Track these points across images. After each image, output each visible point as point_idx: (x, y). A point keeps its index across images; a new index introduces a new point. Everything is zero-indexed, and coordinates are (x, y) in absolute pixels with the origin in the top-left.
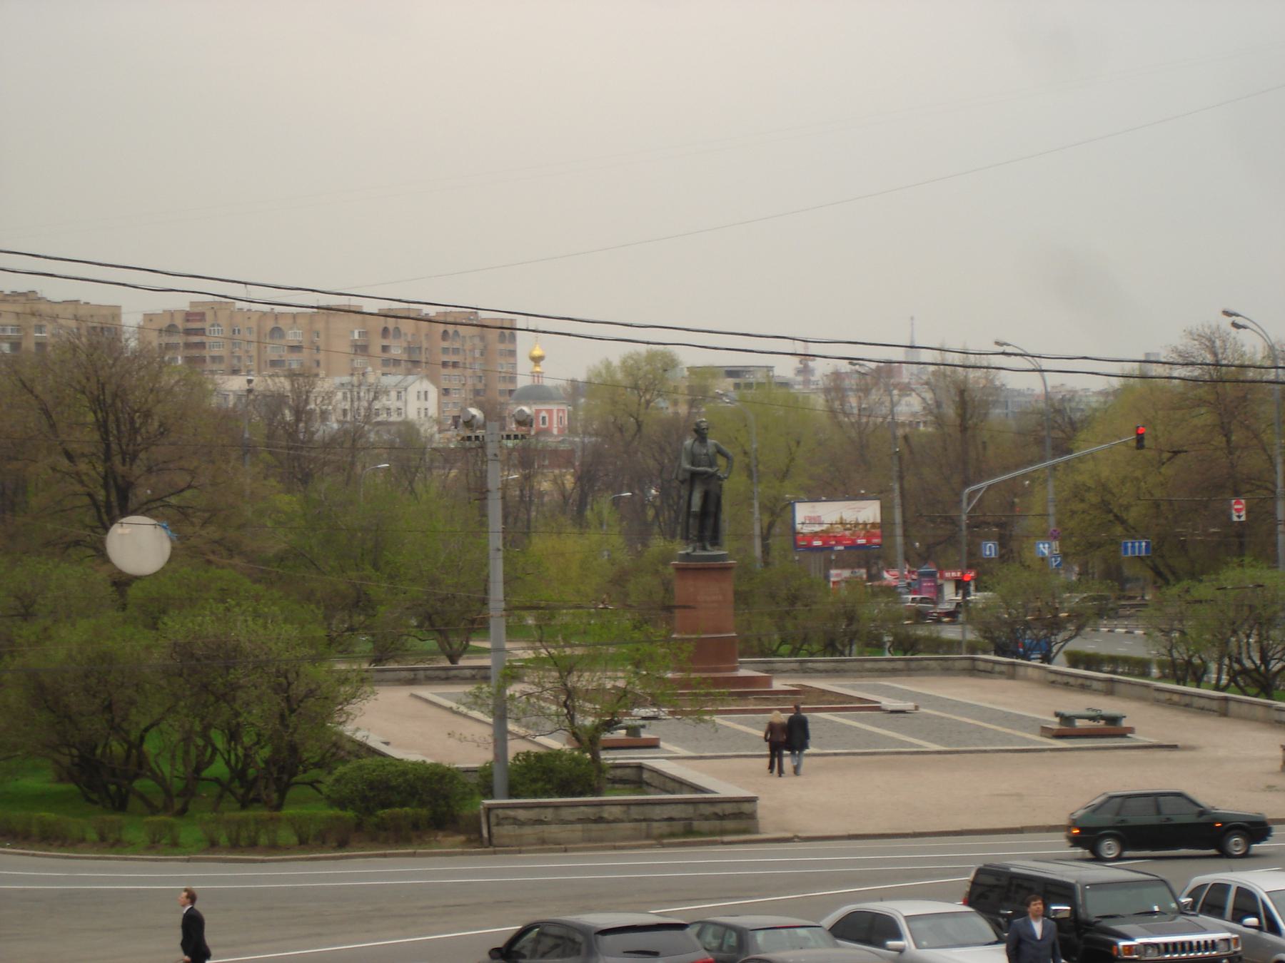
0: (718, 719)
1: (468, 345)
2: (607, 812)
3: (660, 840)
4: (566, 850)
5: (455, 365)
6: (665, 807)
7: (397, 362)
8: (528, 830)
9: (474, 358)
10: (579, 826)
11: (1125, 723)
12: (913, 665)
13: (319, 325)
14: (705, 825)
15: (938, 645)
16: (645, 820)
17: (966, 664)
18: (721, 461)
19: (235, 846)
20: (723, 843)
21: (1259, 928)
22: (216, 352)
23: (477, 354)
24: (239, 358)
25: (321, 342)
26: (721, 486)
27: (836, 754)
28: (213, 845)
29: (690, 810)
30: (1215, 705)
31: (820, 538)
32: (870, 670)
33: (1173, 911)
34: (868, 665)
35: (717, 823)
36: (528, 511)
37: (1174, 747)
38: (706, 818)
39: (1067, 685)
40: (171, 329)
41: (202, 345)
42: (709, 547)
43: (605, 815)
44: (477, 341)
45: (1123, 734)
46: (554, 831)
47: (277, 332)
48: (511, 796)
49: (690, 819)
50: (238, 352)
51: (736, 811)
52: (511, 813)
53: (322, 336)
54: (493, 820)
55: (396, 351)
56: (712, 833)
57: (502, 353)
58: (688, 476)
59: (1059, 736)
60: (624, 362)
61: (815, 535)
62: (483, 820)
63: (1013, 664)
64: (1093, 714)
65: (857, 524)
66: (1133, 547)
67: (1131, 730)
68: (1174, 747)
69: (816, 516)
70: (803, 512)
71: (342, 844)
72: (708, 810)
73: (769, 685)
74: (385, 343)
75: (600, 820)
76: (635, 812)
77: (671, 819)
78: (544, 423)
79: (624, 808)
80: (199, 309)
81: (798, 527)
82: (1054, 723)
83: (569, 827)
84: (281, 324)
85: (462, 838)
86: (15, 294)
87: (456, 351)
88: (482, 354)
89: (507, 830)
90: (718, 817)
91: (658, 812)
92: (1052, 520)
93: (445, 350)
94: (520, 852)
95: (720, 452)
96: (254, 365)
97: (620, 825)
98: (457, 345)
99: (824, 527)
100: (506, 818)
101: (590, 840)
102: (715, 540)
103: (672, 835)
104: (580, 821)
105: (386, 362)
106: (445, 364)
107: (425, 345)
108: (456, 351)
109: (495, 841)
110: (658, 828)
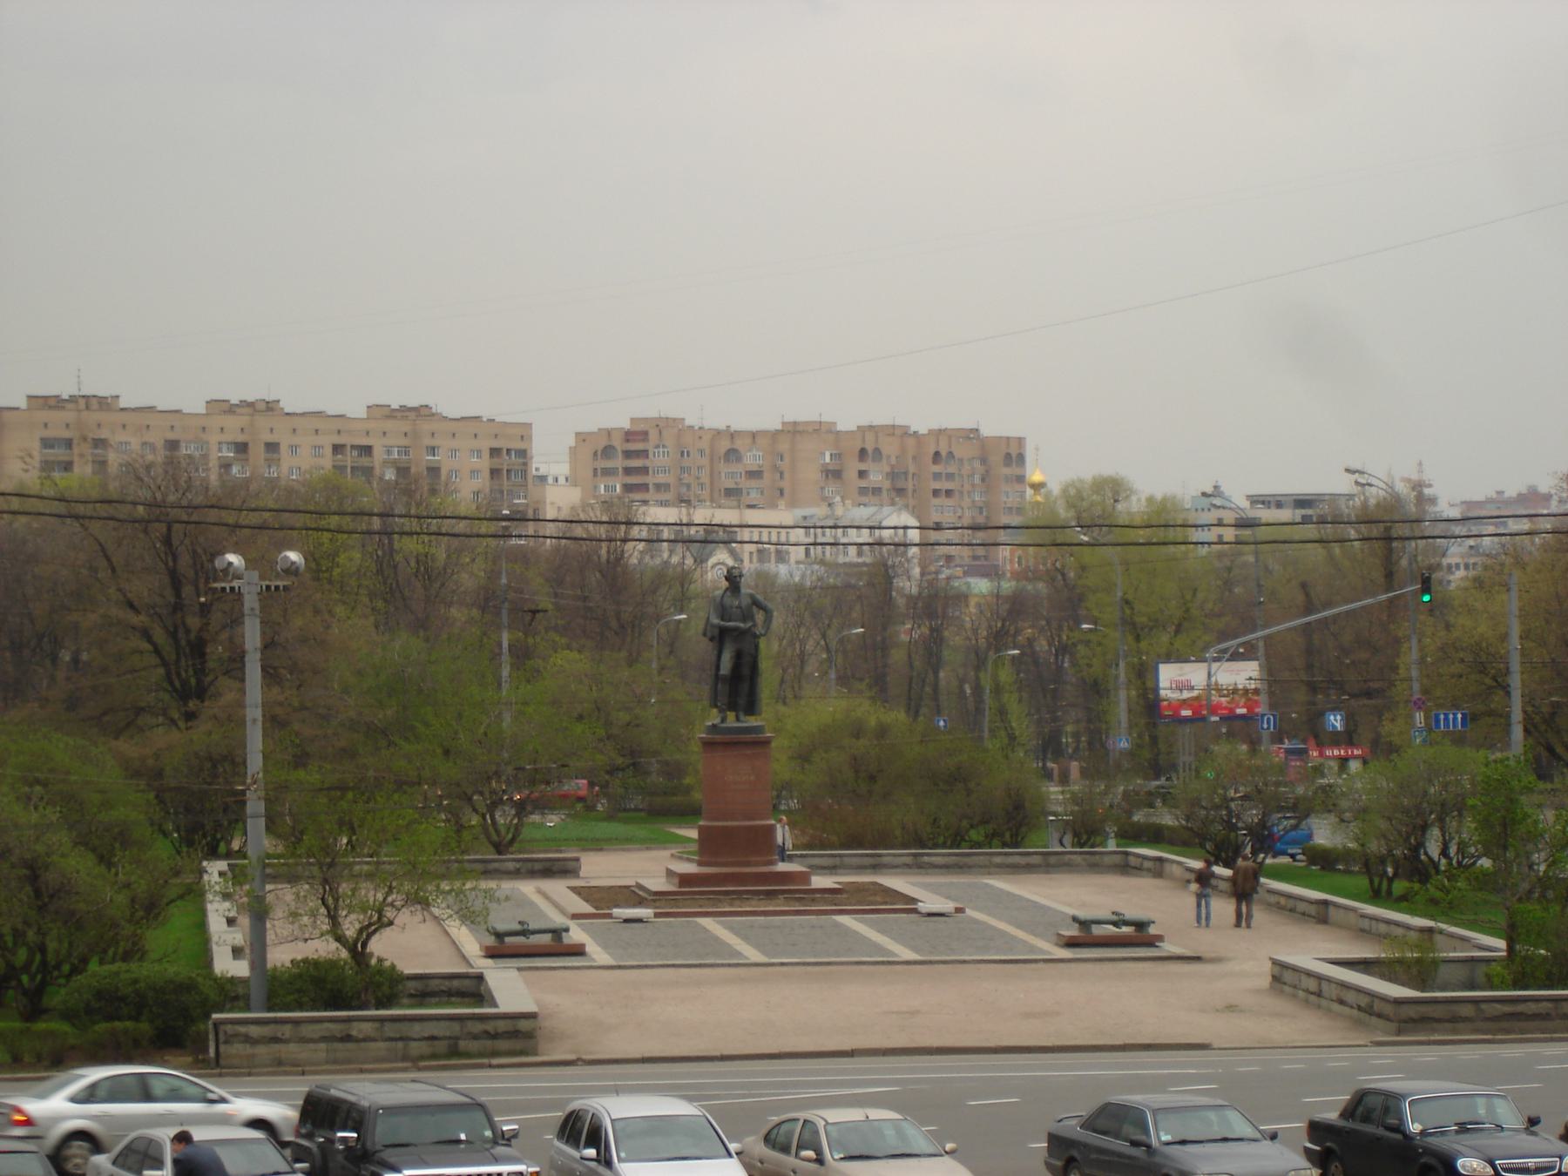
0: (706, 922)
1: (966, 469)
2: (356, 1030)
3: (415, 1062)
4: (303, 1073)
5: (949, 493)
6: (426, 1024)
7: (877, 491)
8: (261, 1050)
9: (973, 485)
10: (323, 1046)
11: (1152, 930)
12: (1053, 860)
13: (784, 446)
14: (474, 1046)
16: (401, 1039)
17: (1117, 859)
18: (760, 617)
20: (490, 1066)
21: (597, 1160)
22: (661, 478)
23: (977, 480)
24: (688, 486)
25: (784, 465)
26: (757, 647)
27: (782, 964)
29: (455, 1028)
30: (1312, 910)
31: (1190, 707)
32: (999, 866)
33: (486, 1140)
34: (998, 860)
35: (489, 1043)
36: (936, 673)
37: (1198, 959)
38: (475, 1037)
40: (608, 451)
41: (644, 471)
42: (742, 717)
43: (354, 1033)
44: (977, 464)
45: (1151, 942)
47: (732, 455)
48: (270, 1010)
49: (457, 1038)
50: (687, 479)
51: (511, 1028)
52: (242, 1029)
53: (787, 460)
54: (222, 1037)
55: (876, 477)
56: (481, 1055)
57: (1008, 479)
58: (716, 632)
59: (1071, 943)
60: (1065, 491)
61: (1184, 703)
62: (211, 1037)
63: (1160, 859)
64: (1115, 918)
65: (1235, 691)
66: (1446, 719)
67: (1160, 938)
68: (1198, 959)
69: (1178, 679)
70: (1168, 674)
72: (478, 1027)
73: (808, 882)
74: (863, 467)
75: (348, 1038)
77: (432, 1038)
79: (377, 1025)
80: (641, 427)
81: (1163, 693)
82: (1073, 931)
83: (312, 1046)
84: (739, 444)
85: (190, 1059)
86: (403, 409)
87: (950, 477)
88: (983, 480)
90: (495, 1036)
91: (417, 1029)
92: (1416, 686)
93: (937, 476)
94: (250, 1074)
95: (755, 603)
96: (706, 493)
97: (372, 1045)
98: (950, 470)
99: (1195, 693)
100: (236, 1035)
101: (335, 1062)
102: (751, 708)
103: (434, 1056)
104: (324, 1039)
105: (863, 491)
106: (936, 493)
107: (912, 469)
108: (950, 477)
109: (222, 1062)
110: (416, 1048)
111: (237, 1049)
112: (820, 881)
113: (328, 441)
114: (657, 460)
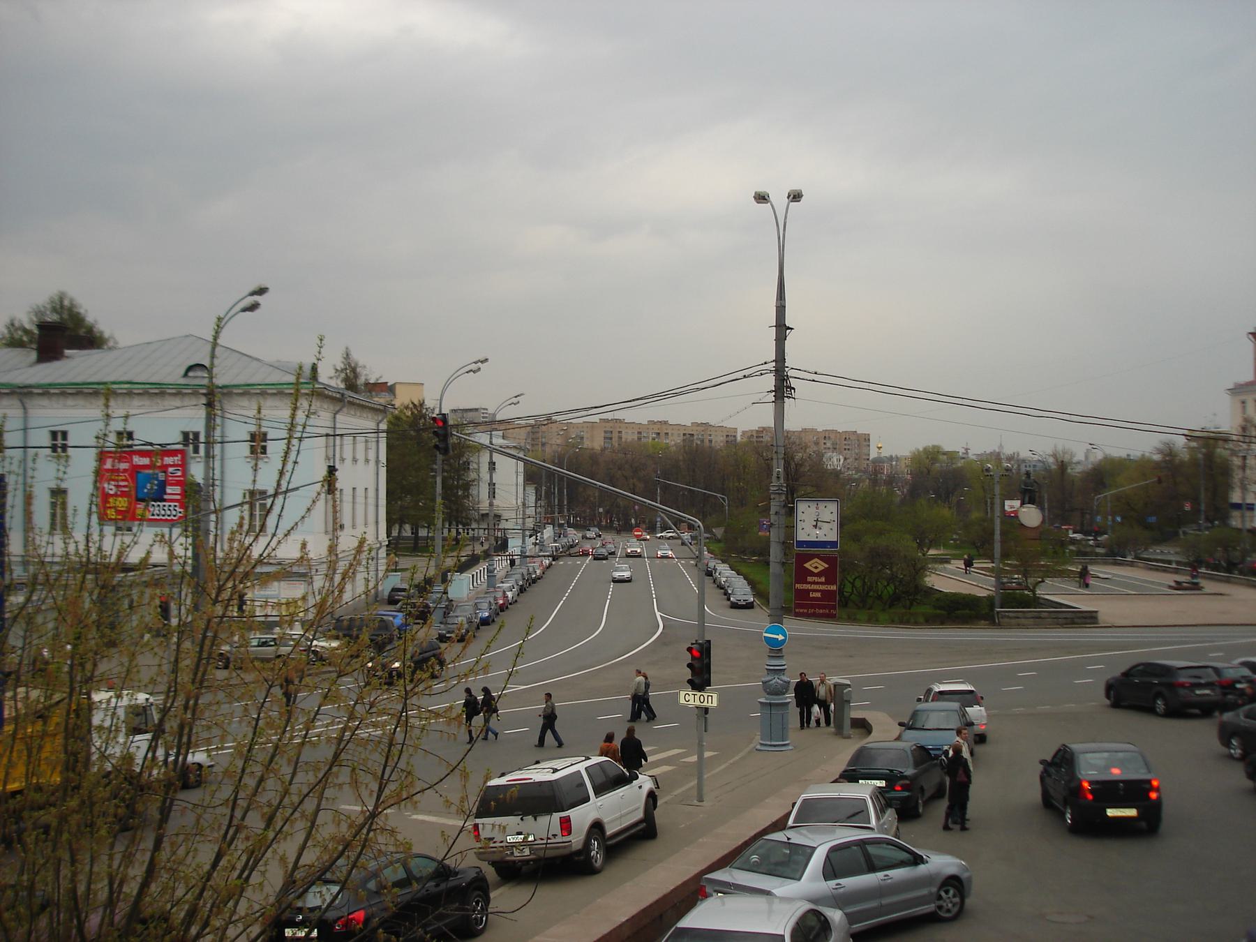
3: (1062, 626)
15: (1097, 555)
19: (901, 622)
28: (893, 622)
39: (63, 394)
46: (1023, 621)
55: (829, 445)
70: (1007, 503)
71: (942, 623)
76: (1053, 615)
78: (60, 521)
82: (1173, 584)
89: (1006, 620)
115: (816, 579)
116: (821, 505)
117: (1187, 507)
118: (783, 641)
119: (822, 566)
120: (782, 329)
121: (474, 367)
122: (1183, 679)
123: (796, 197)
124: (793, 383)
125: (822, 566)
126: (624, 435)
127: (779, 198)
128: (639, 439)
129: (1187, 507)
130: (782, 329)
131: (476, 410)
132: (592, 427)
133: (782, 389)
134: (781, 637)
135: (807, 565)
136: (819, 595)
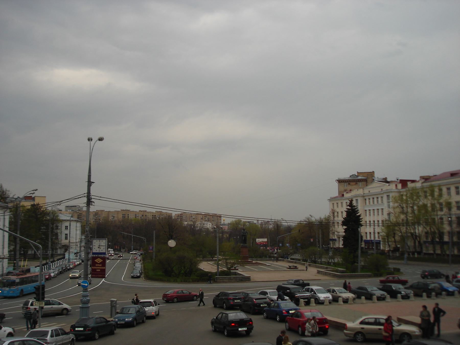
3: (238, 282)
40: (178, 216)
46: (225, 280)
47: (192, 216)
55: (206, 219)
69: (259, 240)
70: (257, 240)
111: (219, 280)
112: (253, 262)
113: (152, 215)
114: (184, 217)
115: (99, 265)
116: (101, 241)
117: (312, 240)
118: (87, 286)
119: (101, 261)
120: (90, 183)
121: (32, 192)
122: (231, 297)
123: (101, 139)
124: (93, 200)
125: (101, 261)
126: (130, 216)
127: (95, 139)
128: (136, 217)
129: (312, 240)
130: (90, 183)
131: (75, 206)
132: (118, 213)
133: (89, 202)
134: (86, 285)
135: (96, 261)
136: (99, 270)
